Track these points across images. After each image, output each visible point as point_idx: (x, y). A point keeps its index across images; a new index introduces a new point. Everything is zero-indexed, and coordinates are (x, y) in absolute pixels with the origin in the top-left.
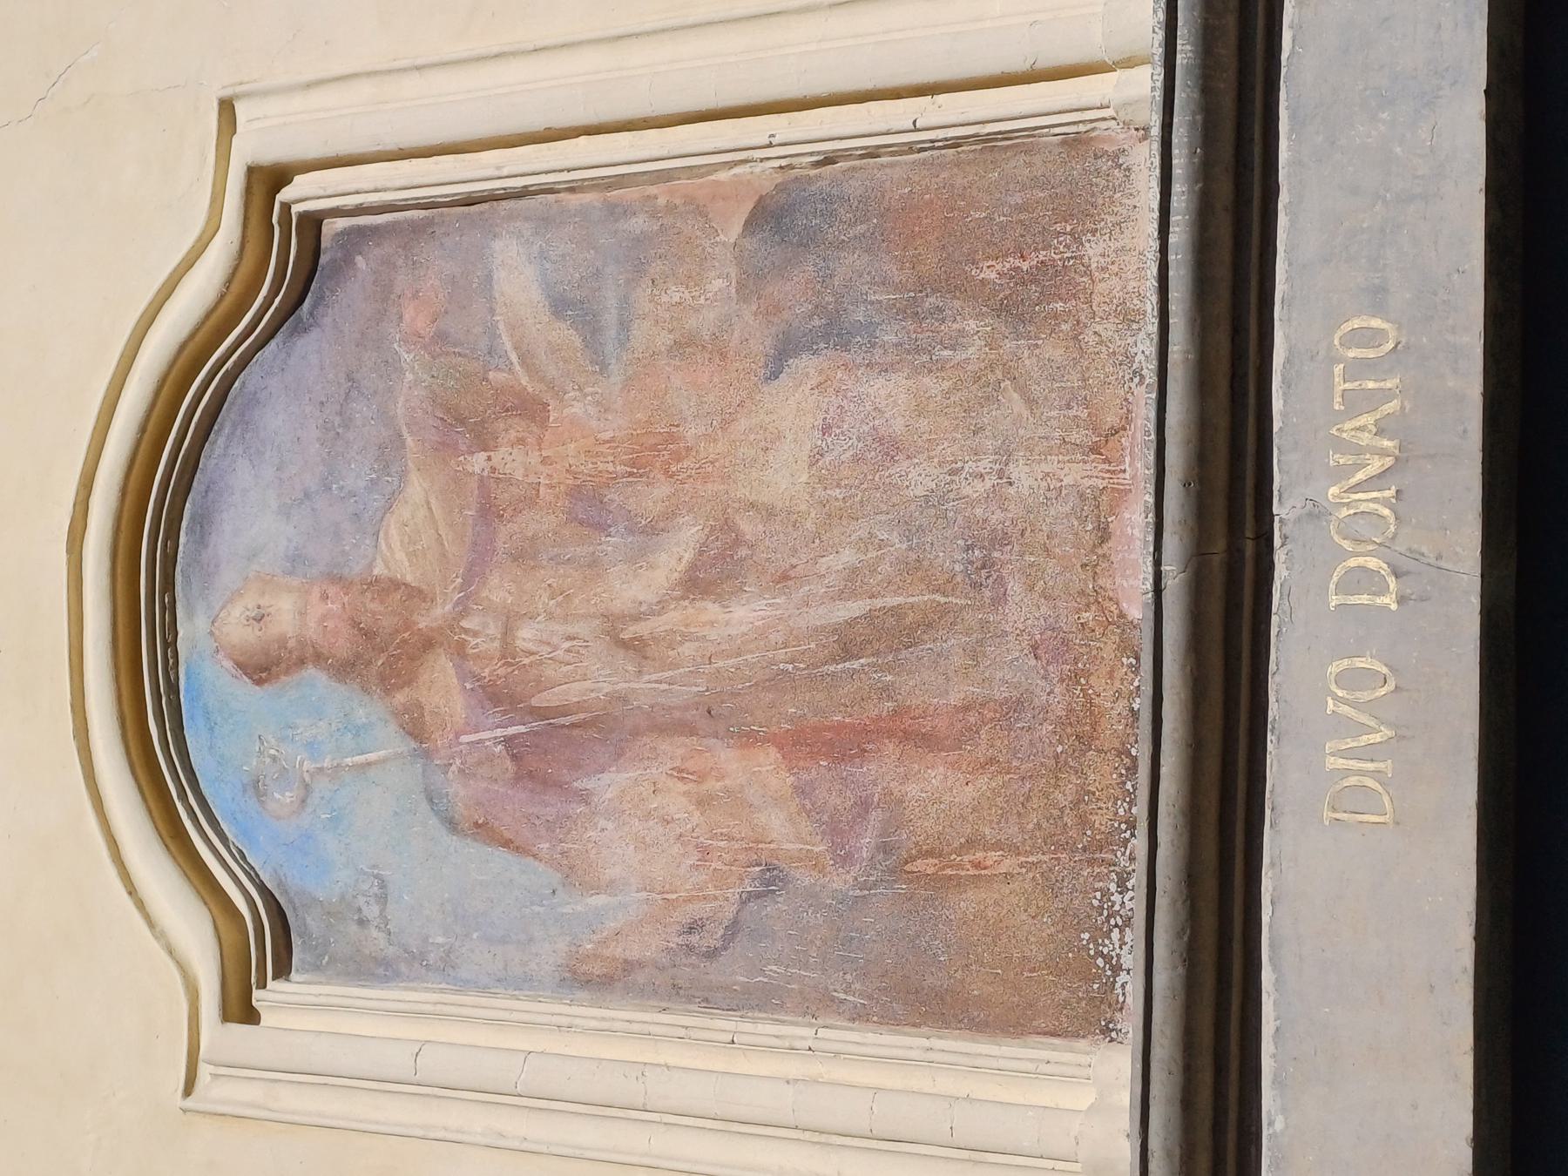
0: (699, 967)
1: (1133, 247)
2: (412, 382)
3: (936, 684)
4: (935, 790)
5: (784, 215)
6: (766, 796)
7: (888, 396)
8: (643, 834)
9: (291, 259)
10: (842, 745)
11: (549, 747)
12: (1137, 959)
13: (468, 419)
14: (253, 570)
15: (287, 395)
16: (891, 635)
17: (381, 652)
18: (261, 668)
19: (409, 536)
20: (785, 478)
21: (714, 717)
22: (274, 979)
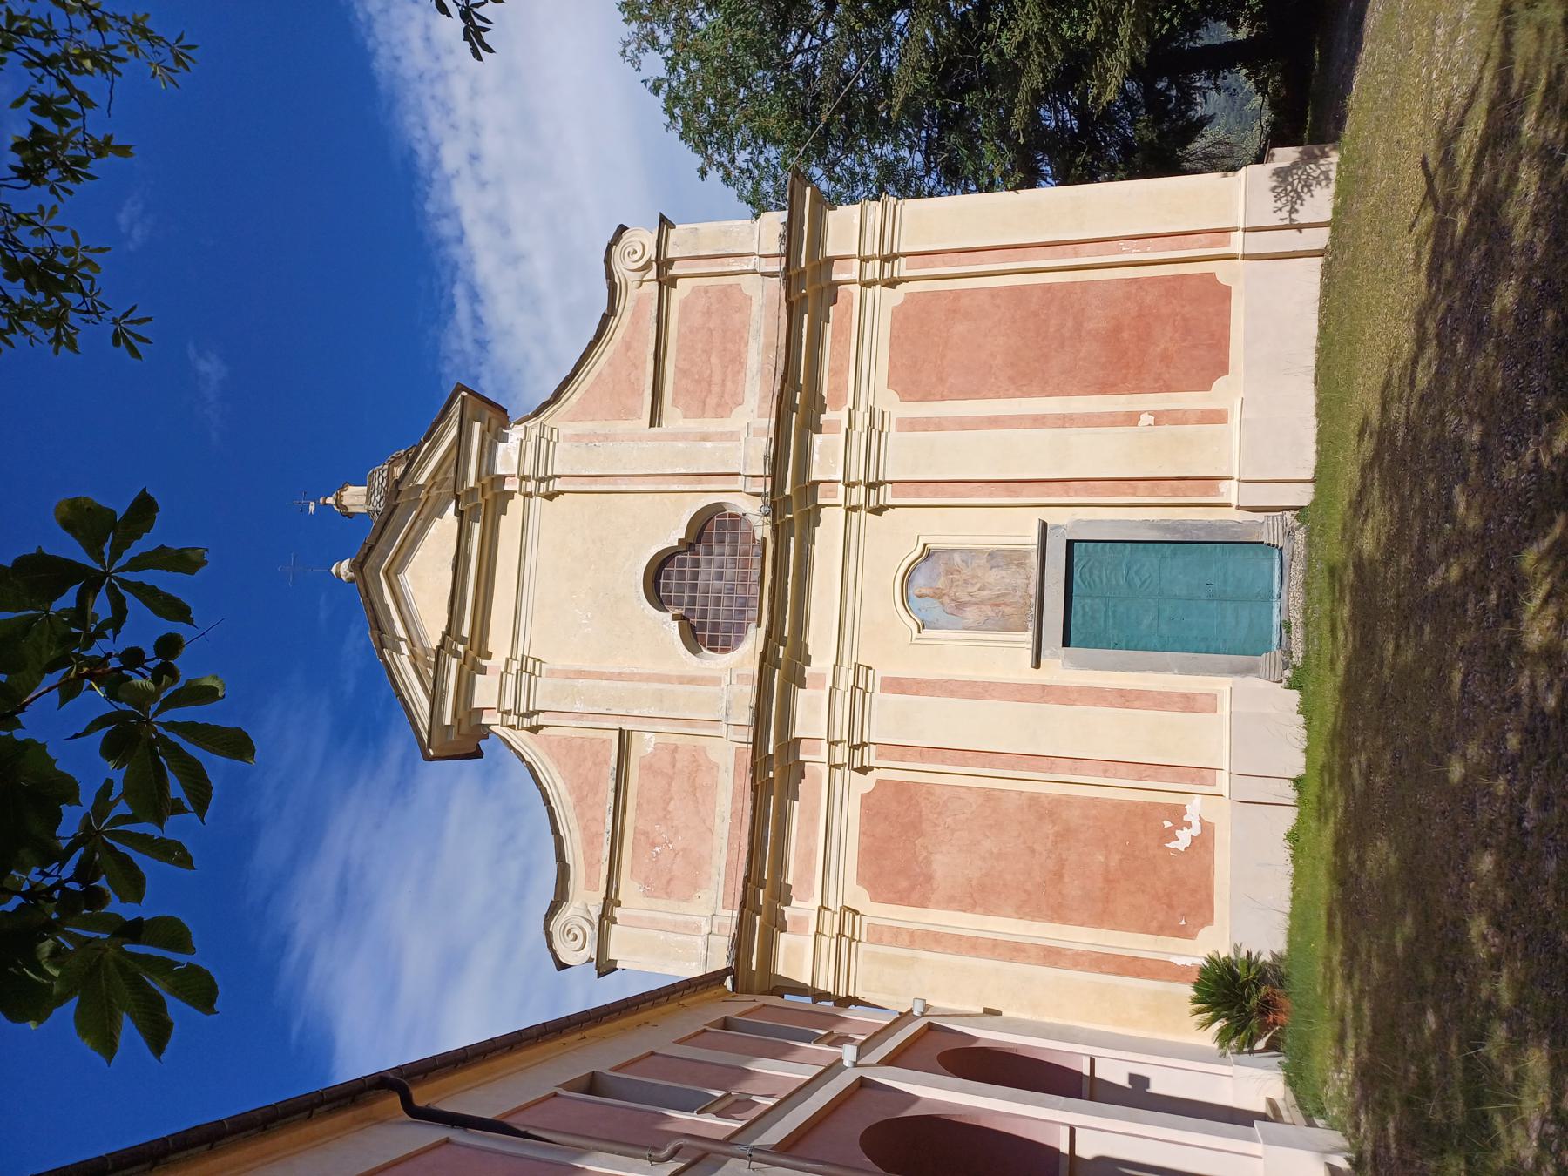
0: (979, 627)
1: (1034, 559)
2: (942, 568)
3: (1007, 600)
4: (1008, 610)
5: (992, 555)
6: (989, 611)
7: (1004, 573)
8: (971, 614)
9: (928, 554)
10: (998, 605)
11: (960, 605)
12: (1032, 626)
13: (949, 572)
14: (920, 582)
15: (925, 569)
16: (1003, 595)
17: (938, 595)
18: (920, 597)
19: (941, 583)
20: (991, 580)
21: (982, 602)
22: (882, 691)
